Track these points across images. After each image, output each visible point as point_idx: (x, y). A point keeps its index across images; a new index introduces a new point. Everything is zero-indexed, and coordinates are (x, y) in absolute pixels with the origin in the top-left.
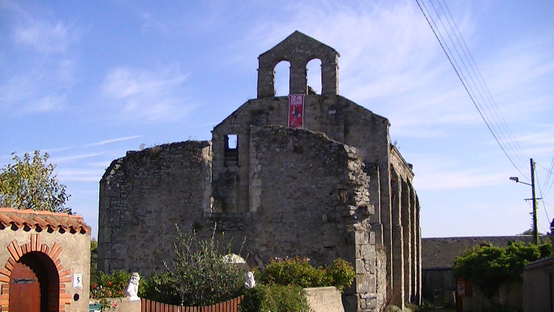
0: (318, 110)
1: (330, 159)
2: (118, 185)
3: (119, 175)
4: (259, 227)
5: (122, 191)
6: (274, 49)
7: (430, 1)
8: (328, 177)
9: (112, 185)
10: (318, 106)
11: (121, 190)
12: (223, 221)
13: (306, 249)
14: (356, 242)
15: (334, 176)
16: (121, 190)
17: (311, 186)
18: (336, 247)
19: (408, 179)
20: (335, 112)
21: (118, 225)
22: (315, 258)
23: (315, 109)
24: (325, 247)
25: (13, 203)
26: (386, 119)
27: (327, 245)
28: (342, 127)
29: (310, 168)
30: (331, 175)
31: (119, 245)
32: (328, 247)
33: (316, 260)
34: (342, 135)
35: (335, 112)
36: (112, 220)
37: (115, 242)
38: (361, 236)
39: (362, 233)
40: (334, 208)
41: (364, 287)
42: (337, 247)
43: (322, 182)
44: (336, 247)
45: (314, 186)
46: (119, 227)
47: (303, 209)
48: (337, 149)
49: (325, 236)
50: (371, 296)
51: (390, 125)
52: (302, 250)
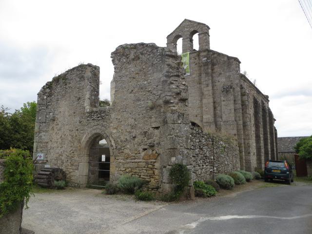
0: (197, 59)
2: (45, 97)
4: (113, 116)
6: (174, 32)
7: (306, 93)
10: (197, 58)
12: (94, 113)
19: (262, 101)
20: (206, 58)
21: (45, 121)
23: (196, 59)
27: (154, 126)
28: (210, 66)
29: (144, 69)
31: (45, 133)
32: (155, 128)
34: (210, 71)
35: (206, 58)
36: (40, 118)
43: (151, 78)
45: (146, 82)
46: (45, 123)
47: (139, 100)
49: (152, 119)
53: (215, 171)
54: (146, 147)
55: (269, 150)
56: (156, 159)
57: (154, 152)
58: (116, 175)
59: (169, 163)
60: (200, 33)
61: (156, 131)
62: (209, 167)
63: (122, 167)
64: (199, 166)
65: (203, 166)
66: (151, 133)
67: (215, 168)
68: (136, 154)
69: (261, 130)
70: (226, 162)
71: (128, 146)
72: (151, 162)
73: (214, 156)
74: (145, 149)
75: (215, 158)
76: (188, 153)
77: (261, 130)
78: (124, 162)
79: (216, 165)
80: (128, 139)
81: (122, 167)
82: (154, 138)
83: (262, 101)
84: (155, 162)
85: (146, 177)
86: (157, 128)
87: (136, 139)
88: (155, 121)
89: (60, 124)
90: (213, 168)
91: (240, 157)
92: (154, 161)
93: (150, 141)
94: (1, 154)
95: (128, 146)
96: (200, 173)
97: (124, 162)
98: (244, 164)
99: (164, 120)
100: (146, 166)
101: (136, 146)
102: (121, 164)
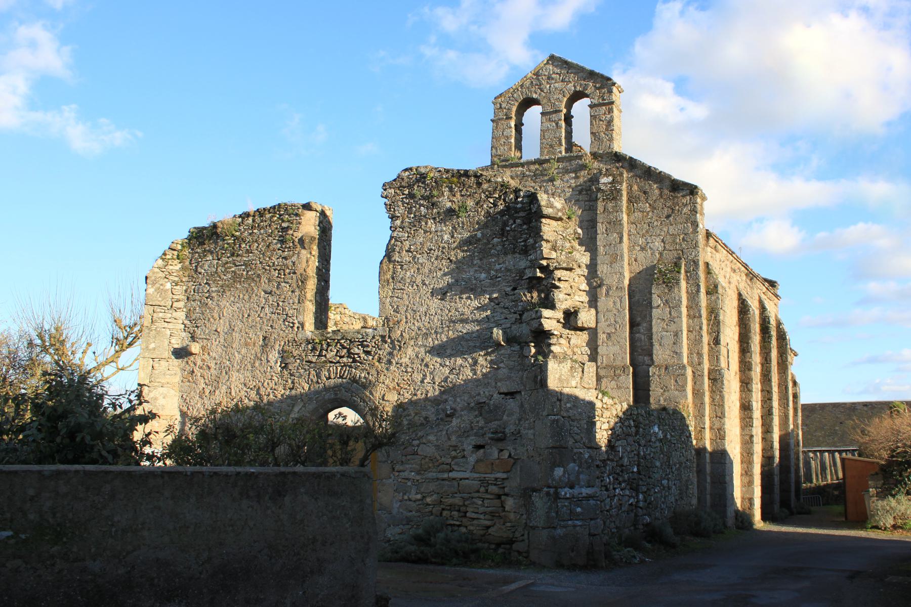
1: (515, 222)
2: (168, 286)
3: (171, 267)
5: (174, 297)
8: (509, 256)
9: (157, 285)
11: (173, 294)
13: (466, 397)
14: (549, 381)
15: (520, 254)
16: (173, 294)
17: (477, 275)
18: (520, 392)
19: (761, 302)
22: (481, 415)
24: (500, 394)
25: (674, 386)
26: (696, 187)
30: (514, 252)
32: (506, 394)
33: (483, 418)
35: (611, 179)
37: (156, 384)
38: (561, 370)
39: (564, 364)
40: (518, 317)
41: (567, 476)
42: (523, 393)
43: (498, 267)
44: (520, 392)
45: (483, 276)
48: (527, 203)
50: (584, 495)
51: (704, 198)
52: (458, 400)
53: (641, 504)
54: (480, 441)
55: (802, 473)
56: (508, 472)
57: (505, 455)
58: (395, 511)
59: (550, 481)
60: (595, 101)
61: (512, 404)
62: (627, 492)
63: (413, 491)
64: (607, 490)
65: (614, 489)
66: (497, 407)
67: (641, 496)
68: (454, 458)
69: (756, 386)
70: (665, 482)
71: (431, 438)
72: (496, 479)
73: (638, 466)
74: (478, 447)
75: (641, 468)
76: (590, 457)
77: (756, 386)
78: (418, 477)
79: (644, 488)
80: (432, 418)
81: (413, 491)
82: (505, 417)
83: (761, 302)
84: (507, 479)
85: (482, 516)
86: (511, 394)
87: (455, 422)
88: (509, 378)
89: (487, 438)
90: (637, 496)
91: (698, 465)
92: (505, 476)
93: (494, 425)
94: (909, 534)
95: (431, 438)
96: (608, 507)
97: (418, 477)
98: (708, 487)
99: (536, 377)
100: (482, 489)
101: (454, 438)
102: (409, 484)
